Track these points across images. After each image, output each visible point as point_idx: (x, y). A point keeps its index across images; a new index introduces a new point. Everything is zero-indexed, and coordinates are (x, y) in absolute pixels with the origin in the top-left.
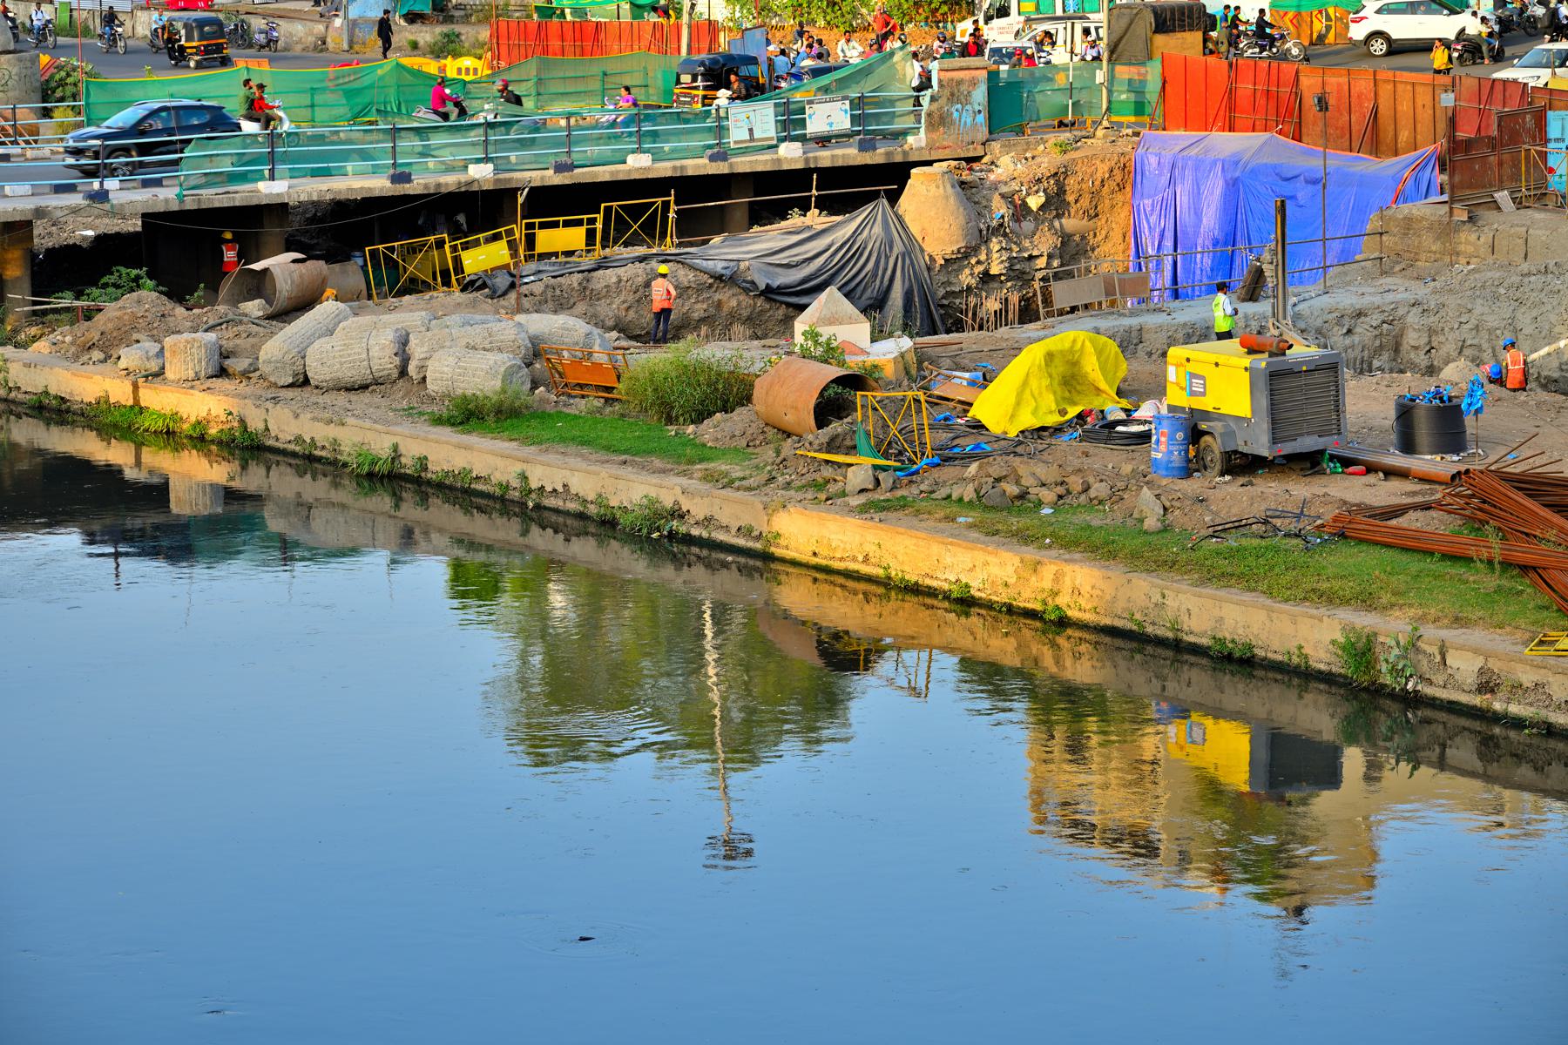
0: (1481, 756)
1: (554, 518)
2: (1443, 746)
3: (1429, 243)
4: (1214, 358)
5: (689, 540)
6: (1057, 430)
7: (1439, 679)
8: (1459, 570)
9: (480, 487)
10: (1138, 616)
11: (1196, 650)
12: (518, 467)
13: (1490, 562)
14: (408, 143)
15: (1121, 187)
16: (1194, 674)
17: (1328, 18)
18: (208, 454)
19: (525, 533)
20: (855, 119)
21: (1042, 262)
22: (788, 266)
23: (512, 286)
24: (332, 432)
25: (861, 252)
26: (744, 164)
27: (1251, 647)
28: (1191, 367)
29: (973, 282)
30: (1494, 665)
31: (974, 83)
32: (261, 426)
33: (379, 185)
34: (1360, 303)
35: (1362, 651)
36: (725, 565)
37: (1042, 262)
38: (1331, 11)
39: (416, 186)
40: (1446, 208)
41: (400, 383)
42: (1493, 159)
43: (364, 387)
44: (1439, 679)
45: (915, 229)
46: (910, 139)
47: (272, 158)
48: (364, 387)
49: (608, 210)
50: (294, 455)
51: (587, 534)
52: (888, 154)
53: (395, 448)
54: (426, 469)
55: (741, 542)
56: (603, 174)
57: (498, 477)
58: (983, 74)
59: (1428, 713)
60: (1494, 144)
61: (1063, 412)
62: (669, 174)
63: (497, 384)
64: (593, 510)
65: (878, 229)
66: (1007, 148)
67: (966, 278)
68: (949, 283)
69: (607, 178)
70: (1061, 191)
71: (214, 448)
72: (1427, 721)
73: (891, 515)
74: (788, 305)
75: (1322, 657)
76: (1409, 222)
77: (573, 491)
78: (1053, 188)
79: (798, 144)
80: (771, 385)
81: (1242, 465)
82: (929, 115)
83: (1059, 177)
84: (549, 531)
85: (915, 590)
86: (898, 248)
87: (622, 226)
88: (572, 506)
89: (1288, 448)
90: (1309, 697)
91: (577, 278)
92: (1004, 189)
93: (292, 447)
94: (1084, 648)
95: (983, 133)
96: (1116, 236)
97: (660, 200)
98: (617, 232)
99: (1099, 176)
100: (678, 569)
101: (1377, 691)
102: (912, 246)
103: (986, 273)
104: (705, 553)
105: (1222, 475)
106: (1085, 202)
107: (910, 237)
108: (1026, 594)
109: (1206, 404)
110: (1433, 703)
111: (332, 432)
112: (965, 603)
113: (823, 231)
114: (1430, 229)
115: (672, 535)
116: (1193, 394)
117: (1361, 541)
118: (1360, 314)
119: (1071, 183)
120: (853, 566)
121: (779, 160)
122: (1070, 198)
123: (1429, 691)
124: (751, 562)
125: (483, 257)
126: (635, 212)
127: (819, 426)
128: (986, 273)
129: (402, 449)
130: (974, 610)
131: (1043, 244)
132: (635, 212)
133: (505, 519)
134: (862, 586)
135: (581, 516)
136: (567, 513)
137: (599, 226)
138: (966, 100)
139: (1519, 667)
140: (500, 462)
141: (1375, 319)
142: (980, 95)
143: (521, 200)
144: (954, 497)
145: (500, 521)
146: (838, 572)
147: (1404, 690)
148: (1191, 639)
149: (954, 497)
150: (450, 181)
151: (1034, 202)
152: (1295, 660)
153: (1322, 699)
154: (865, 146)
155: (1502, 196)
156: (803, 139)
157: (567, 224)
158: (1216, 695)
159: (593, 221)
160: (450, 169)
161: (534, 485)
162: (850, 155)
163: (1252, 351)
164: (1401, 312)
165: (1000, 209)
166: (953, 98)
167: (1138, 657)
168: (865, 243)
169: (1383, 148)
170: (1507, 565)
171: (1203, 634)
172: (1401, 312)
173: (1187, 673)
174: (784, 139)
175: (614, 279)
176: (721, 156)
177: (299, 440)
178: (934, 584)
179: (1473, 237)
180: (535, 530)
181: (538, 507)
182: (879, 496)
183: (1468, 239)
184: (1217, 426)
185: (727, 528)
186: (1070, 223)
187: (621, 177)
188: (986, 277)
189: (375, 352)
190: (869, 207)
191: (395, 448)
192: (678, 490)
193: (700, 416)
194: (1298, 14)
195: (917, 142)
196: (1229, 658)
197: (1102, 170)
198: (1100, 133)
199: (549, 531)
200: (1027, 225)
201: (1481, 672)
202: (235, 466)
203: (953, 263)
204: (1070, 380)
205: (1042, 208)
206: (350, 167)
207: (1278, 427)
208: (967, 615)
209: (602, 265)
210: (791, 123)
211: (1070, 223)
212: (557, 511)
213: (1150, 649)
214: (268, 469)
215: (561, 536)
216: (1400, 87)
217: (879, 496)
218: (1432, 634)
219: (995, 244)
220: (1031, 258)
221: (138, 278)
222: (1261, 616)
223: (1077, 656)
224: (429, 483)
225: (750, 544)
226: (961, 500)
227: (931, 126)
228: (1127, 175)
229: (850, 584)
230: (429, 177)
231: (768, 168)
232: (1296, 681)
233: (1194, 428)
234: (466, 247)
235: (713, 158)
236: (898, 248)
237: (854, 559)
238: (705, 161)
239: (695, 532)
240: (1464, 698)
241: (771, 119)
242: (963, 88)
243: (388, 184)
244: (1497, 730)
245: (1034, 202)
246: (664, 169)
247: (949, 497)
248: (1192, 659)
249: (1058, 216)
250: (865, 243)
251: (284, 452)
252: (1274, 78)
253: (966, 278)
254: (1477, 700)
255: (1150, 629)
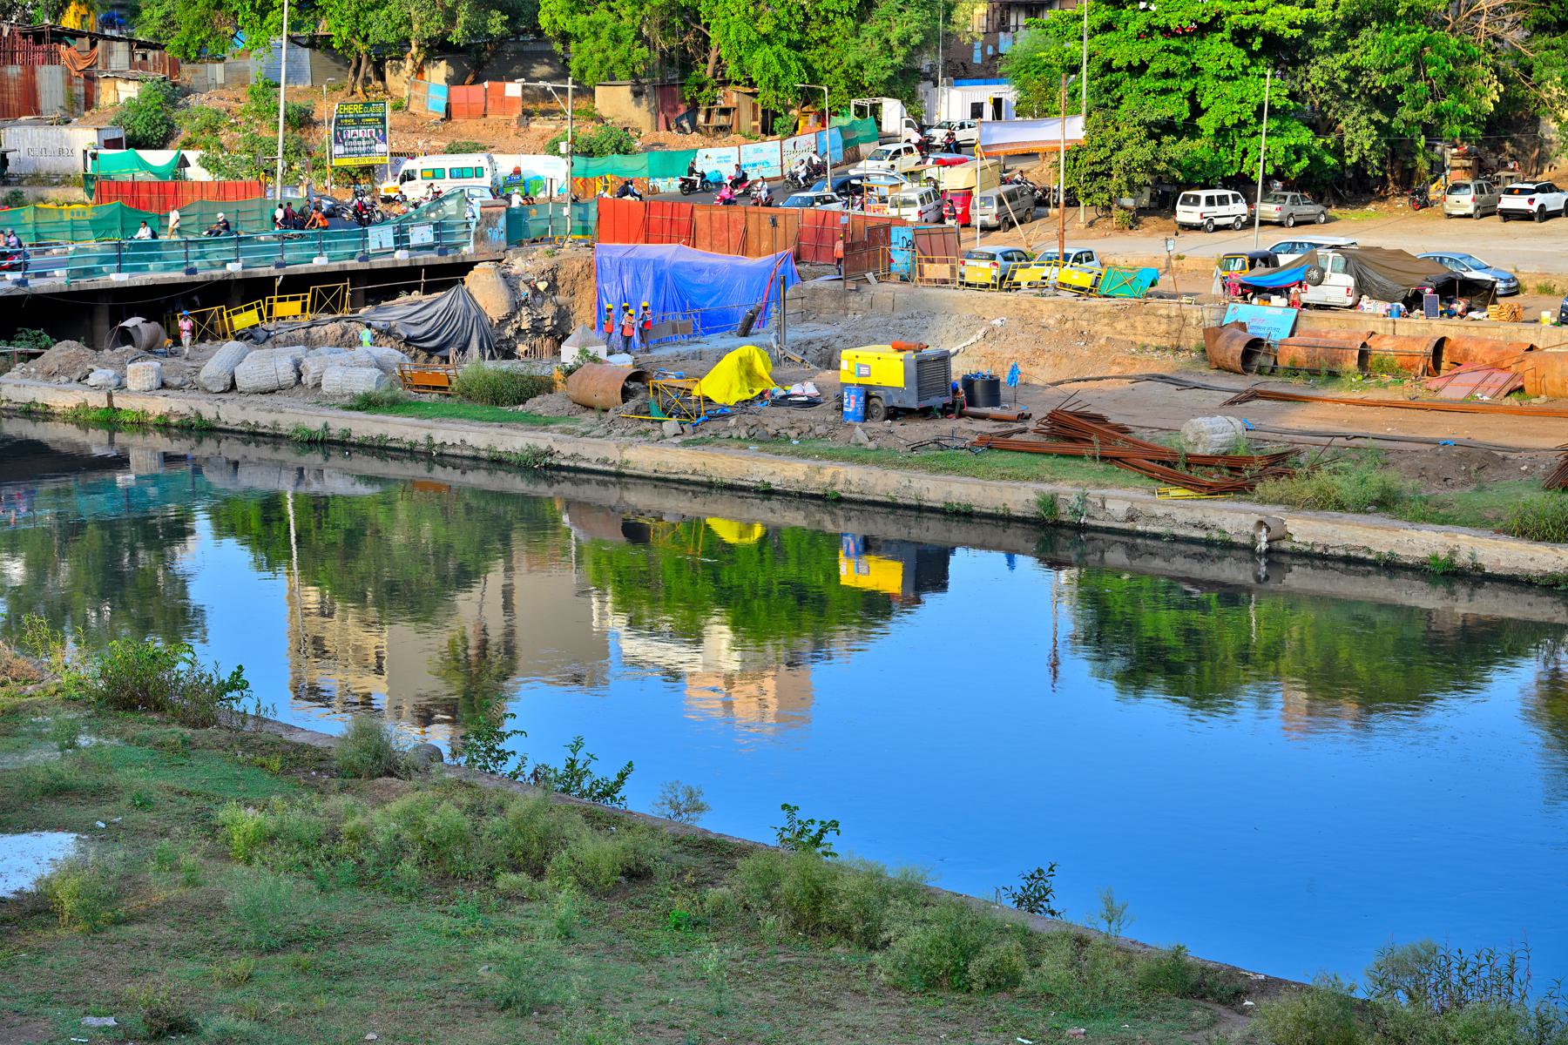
0: (1128, 556)
1: (453, 460)
2: (1103, 552)
3: (830, 303)
4: (878, 355)
5: (559, 468)
6: (752, 401)
7: (1101, 515)
8: (1079, 462)
9: (393, 445)
10: (892, 494)
11: (932, 510)
12: (425, 432)
13: (1094, 458)
14: (194, 250)
15: (588, 277)
16: (931, 524)
17: (606, 181)
18: (168, 435)
19: (430, 470)
20: (437, 236)
21: (548, 322)
22: (416, 324)
23: (268, 337)
24: (274, 416)
25: (453, 316)
26: (378, 263)
27: (970, 506)
28: (859, 361)
29: (513, 334)
30: (1138, 506)
31: (499, 215)
32: (213, 416)
33: (178, 276)
34: (811, 336)
35: (1051, 503)
36: (588, 481)
37: (548, 322)
38: (608, 177)
39: (199, 277)
40: (841, 283)
41: (297, 389)
42: (865, 254)
43: (273, 392)
44: (1101, 515)
45: (480, 302)
46: (465, 249)
47: (119, 259)
48: (273, 392)
49: (314, 290)
50: (241, 432)
51: (479, 468)
52: (454, 257)
53: (326, 425)
54: (349, 436)
55: (600, 467)
56: (302, 269)
57: (408, 438)
58: (503, 210)
59: (1092, 534)
60: (866, 246)
61: (751, 392)
62: (337, 269)
63: (373, 386)
64: (484, 454)
65: (461, 302)
66: (517, 255)
67: (509, 332)
68: (499, 335)
69: (304, 272)
70: (555, 279)
71: (175, 431)
72: (1093, 539)
73: (700, 448)
74: (417, 347)
75: (1017, 509)
76: (815, 291)
77: (469, 443)
78: (550, 278)
79: (406, 252)
80: (582, 380)
81: (894, 413)
82: (475, 234)
83: (554, 271)
84: (449, 469)
85: (731, 488)
86: (474, 313)
87: (321, 301)
88: (466, 453)
89: (925, 404)
90: (1009, 531)
91: (302, 332)
92: (524, 278)
93: (239, 428)
94: (852, 514)
95: (504, 245)
96: (586, 306)
97: (342, 285)
98: (319, 305)
99: (576, 270)
100: (551, 485)
101: (1059, 525)
102: (481, 313)
103: (519, 328)
104: (572, 475)
105: (885, 419)
106: (568, 286)
107: (479, 307)
108: (812, 485)
109: (872, 381)
110: (1096, 529)
111: (274, 416)
112: (767, 493)
113: (432, 303)
114: (829, 295)
115: (547, 466)
116: (860, 375)
117: (1002, 450)
118: (810, 343)
119: (560, 274)
120: (686, 477)
121: (396, 261)
122: (559, 284)
123: (1093, 523)
124: (607, 478)
125: (245, 319)
126: (329, 291)
127: (624, 402)
128: (519, 328)
129: (331, 425)
130: (773, 497)
131: (548, 311)
132: (329, 291)
133: (414, 463)
134: (692, 488)
135: (475, 458)
136: (464, 457)
137: (309, 300)
138: (494, 225)
139: (1154, 506)
140: (410, 430)
141: (818, 346)
142: (502, 222)
143: (278, 283)
144: (735, 436)
145: (409, 464)
146: (674, 481)
147: (1079, 523)
148: (930, 504)
149: (735, 436)
150: (218, 273)
151: (542, 286)
152: (1001, 512)
153: (1019, 532)
154: (442, 252)
155: (870, 276)
156: (408, 248)
157: (291, 299)
158: (947, 534)
159: (305, 297)
160: (212, 266)
161: (437, 441)
162: (432, 258)
163: (900, 350)
164: (832, 341)
165: (525, 291)
166: (488, 224)
167: (892, 517)
168: (456, 310)
169: (750, 251)
170: (1103, 458)
171: (938, 501)
172: (832, 341)
173: (926, 523)
174: (397, 248)
175: (323, 333)
176: (364, 259)
177: (245, 423)
178: (745, 483)
179: (858, 299)
180: (437, 468)
181: (440, 455)
182: (686, 438)
183: (853, 300)
184: (882, 393)
185: (588, 460)
186: (560, 298)
187: (312, 271)
188: (519, 331)
189: (281, 370)
190: (454, 289)
191: (326, 425)
192: (551, 440)
193: (521, 401)
194: (585, 180)
195: (468, 250)
196: (957, 513)
197: (577, 266)
198: (567, 245)
199: (449, 469)
200: (538, 300)
201: (1129, 510)
202: (193, 441)
203: (503, 322)
204: (749, 374)
205: (546, 290)
206: (151, 265)
207: (922, 392)
208: (769, 499)
209: (314, 324)
210: (401, 240)
211: (560, 298)
212: (455, 456)
213: (900, 512)
214: (219, 442)
215: (459, 471)
216: (763, 216)
217: (686, 438)
218: (1094, 493)
219: (524, 311)
220: (543, 319)
221: (40, 335)
222: (978, 489)
223: (848, 519)
224: (353, 444)
225: (607, 468)
226: (739, 438)
227: (477, 241)
228: (593, 270)
229: (683, 487)
230: (205, 272)
231: (390, 266)
232: (1001, 523)
233: (868, 395)
234: (235, 313)
235: (361, 260)
236: (474, 313)
237: (686, 473)
238: (273, 268)
239: (564, 463)
240: (1117, 525)
241: (392, 236)
242: (494, 218)
243: (184, 275)
244: (1139, 541)
245: (542, 286)
246: (335, 266)
247: (731, 437)
248: (930, 515)
249: (554, 294)
250: (456, 310)
251: (233, 431)
252: (676, 212)
253: (509, 332)
254: (1128, 526)
255: (900, 501)
